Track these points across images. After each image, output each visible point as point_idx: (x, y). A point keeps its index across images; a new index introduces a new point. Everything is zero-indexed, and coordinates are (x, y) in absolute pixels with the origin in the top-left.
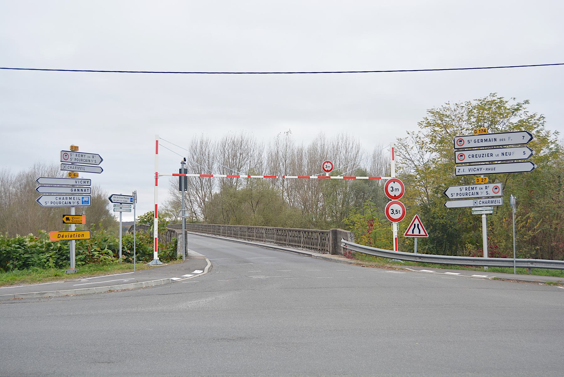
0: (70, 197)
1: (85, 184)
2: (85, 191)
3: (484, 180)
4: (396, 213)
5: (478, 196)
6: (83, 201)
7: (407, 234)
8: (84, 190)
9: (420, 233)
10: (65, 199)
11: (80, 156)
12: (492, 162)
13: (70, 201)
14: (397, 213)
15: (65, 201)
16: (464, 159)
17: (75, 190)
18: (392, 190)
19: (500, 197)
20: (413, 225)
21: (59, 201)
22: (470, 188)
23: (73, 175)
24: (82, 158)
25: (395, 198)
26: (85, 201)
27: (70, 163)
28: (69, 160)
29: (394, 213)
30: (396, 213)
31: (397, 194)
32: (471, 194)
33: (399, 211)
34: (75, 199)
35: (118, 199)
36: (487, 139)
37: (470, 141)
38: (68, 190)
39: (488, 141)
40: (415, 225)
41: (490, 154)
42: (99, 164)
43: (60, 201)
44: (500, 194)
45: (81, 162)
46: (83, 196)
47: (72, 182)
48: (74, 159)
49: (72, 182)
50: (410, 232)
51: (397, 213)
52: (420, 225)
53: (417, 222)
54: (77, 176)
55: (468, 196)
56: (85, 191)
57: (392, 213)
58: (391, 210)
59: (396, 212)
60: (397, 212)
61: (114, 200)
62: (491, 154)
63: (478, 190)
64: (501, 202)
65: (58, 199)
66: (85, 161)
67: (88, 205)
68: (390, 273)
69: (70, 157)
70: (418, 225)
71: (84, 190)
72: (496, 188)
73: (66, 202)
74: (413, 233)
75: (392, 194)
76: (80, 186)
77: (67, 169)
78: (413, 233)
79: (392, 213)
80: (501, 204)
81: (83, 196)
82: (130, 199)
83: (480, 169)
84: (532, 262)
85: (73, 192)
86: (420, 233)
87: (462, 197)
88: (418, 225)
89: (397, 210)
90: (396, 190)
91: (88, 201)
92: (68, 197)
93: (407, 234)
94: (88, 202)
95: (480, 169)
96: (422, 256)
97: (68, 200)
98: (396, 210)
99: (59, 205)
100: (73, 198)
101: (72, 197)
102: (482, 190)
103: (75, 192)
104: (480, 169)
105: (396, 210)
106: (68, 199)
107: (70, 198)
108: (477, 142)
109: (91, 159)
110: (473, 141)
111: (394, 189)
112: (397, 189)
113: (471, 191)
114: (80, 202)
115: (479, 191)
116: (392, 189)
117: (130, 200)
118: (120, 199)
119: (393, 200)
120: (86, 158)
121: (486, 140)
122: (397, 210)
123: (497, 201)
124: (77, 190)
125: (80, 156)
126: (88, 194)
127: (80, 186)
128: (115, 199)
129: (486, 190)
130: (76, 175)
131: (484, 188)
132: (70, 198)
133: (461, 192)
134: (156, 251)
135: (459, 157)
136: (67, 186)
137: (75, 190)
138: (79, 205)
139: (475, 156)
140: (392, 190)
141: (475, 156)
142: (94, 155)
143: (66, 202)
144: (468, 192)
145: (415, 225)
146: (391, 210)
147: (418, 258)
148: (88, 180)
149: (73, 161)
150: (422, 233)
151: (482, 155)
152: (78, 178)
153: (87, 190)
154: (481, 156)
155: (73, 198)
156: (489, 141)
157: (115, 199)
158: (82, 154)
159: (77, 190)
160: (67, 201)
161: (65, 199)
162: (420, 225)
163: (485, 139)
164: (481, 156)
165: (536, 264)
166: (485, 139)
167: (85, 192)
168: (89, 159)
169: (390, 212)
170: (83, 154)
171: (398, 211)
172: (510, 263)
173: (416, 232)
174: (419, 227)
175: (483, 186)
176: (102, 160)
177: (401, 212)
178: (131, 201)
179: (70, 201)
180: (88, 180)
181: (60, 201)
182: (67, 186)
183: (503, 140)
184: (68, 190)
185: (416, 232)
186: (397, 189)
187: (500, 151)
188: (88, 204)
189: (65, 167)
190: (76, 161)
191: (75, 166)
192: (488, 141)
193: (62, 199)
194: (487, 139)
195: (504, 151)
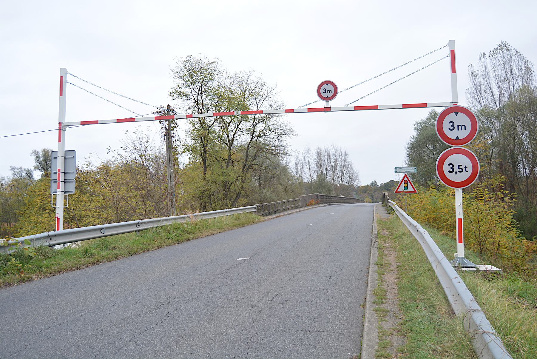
4: (459, 171)
7: (398, 191)
14: (461, 170)
18: (325, 92)
25: (457, 142)
30: (459, 171)
31: (462, 134)
33: (466, 167)
51: (461, 170)
57: (451, 170)
58: (449, 165)
59: (459, 168)
60: (461, 169)
68: (61, 177)
75: (452, 135)
79: (451, 170)
89: (461, 166)
90: (329, 91)
93: (398, 191)
98: (459, 166)
105: (459, 166)
111: (327, 91)
112: (329, 91)
119: (454, 147)
122: (461, 166)
134: (460, 242)
140: (325, 92)
146: (449, 165)
169: (446, 168)
171: (463, 167)
172: (211, 215)
177: (470, 169)
186: (462, 126)
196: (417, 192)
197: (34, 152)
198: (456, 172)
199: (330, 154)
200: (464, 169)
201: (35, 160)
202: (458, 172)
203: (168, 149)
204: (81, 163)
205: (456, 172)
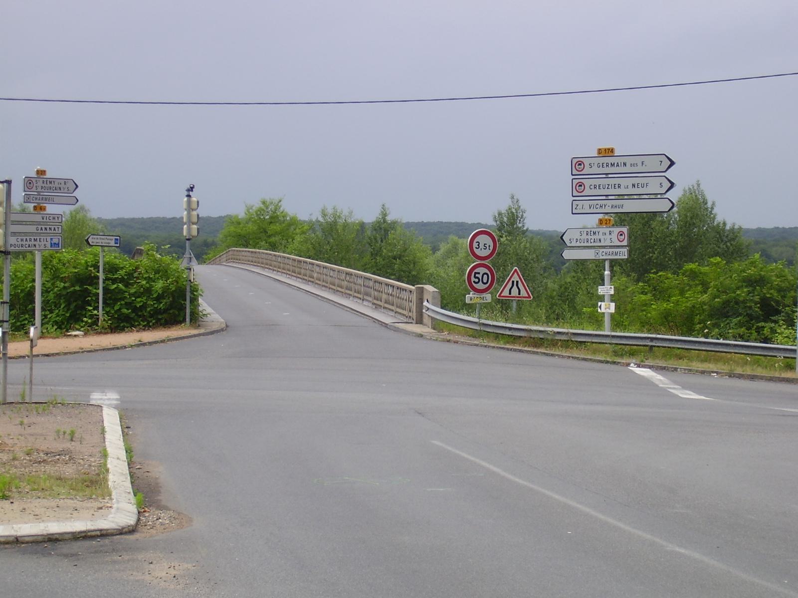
0: (35, 238)
1: (54, 221)
2: (55, 230)
3: (608, 221)
4: (484, 249)
5: (600, 244)
6: (51, 243)
7: (527, 296)
8: (52, 229)
9: (519, 294)
10: (28, 240)
11: (48, 182)
12: (621, 197)
13: (35, 243)
14: (485, 248)
15: (28, 243)
16: (584, 190)
17: (46, 229)
19: (625, 246)
20: (511, 282)
21: (20, 243)
22: (592, 233)
23: (39, 208)
24: (50, 185)
26: (55, 244)
27: (36, 193)
28: (34, 189)
29: (480, 248)
30: (484, 249)
32: (592, 241)
33: (489, 246)
34: (42, 240)
35: (98, 241)
36: (614, 164)
37: (592, 165)
38: (32, 229)
39: (616, 165)
40: (513, 282)
41: (617, 185)
42: (74, 191)
43: (22, 243)
44: (625, 243)
45: (49, 191)
46: (52, 237)
47: (38, 218)
48: (40, 187)
49: (38, 218)
50: (506, 293)
52: (520, 282)
53: (515, 278)
54: (45, 209)
55: (589, 244)
56: (55, 230)
57: (478, 247)
58: (477, 242)
61: (93, 242)
62: (618, 184)
63: (601, 236)
64: (626, 254)
65: (19, 240)
66: (54, 189)
67: (58, 249)
69: (35, 185)
70: (517, 282)
71: (52, 229)
72: (621, 235)
73: (29, 245)
74: (510, 293)
76: (53, 224)
77: (32, 201)
78: (510, 293)
80: (626, 257)
81: (52, 237)
82: (114, 240)
83: (603, 206)
84: (652, 339)
85: (39, 231)
86: (519, 294)
87: (582, 244)
88: (517, 282)
89: (479, 273)
91: (59, 243)
92: (33, 238)
93: (527, 296)
94: (58, 244)
95: (603, 206)
96: (512, 327)
97: (33, 242)
98: (485, 244)
99: (20, 248)
100: (38, 240)
101: (38, 238)
102: (604, 237)
103: (42, 231)
104: (603, 206)
105: (485, 244)
106: (33, 240)
107: (36, 240)
108: (601, 166)
109: (62, 186)
110: (596, 165)
113: (593, 237)
114: (48, 245)
115: (602, 237)
116: (478, 245)
117: (113, 241)
118: (100, 241)
120: (56, 185)
121: (613, 163)
123: (621, 253)
124: (44, 229)
125: (48, 182)
126: (58, 235)
127: (53, 224)
128: (94, 240)
129: (610, 237)
130: (43, 209)
131: (608, 233)
132: (34, 239)
133: (581, 237)
135: (577, 188)
136: (32, 223)
137: (46, 229)
138: (47, 248)
139: (597, 188)
141: (597, 188)
142: (66, 181)
143: (29, 245)
144: (589, 237)
145: (513, 282)
146: (477, 242)
147: (507, 330)
148: (58, 216)
149: (39, 190)
150: (524, 293)
151: (607, 186)
152: (45, 213)
153: (57, 229)
154: (606, 188)
155: (38, 240)
156: (617, 166)
157: (94, 240)
158: (50, 180)
159: (44, 229)
160: (30, 243)
161: (28, 240)
162: (520, 282)
163: (611, 164)
164: (606, 188)
165: (656, 341)
166: (611, 164)
167: (55, 232)
168: (60, 186)
169: (475, 245)
170: (51, 181)
171: (487, 246)
173: (515, 292)
174: (519, 285)
175: (607, 230)
176: (77, 186)
177: (491, 248)
178: (115, 243)
179: (35, 243)
180: (58, 216)
181: (22, 243)
182: (32, 223)
183: (635, 165)
184: (32, 229)
185: (515, 292)
187: (630, 182)
188: (59, 247)
189: (29, 198)
190: (43, 190)
191: (41, 197)
192: (616, 165)
193: (24, 240)
194: (614, 164)
195: (635, 181)
196: (532, 297)
197: (512, 194)
198: (481, 249)
199: (100, 345)
200: (488, 247)
201: (257, 205)
202: (483, 249)
203: (83, 534)
204: (386, 217)
205: (481, 249)
